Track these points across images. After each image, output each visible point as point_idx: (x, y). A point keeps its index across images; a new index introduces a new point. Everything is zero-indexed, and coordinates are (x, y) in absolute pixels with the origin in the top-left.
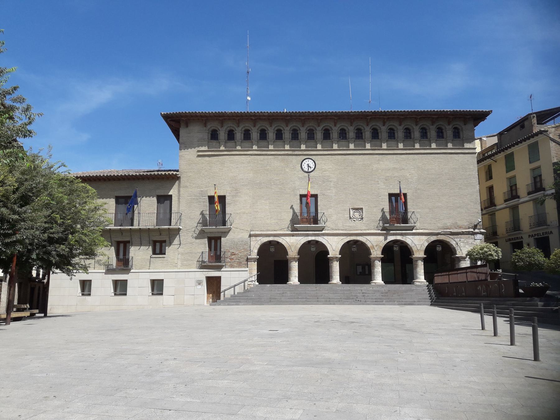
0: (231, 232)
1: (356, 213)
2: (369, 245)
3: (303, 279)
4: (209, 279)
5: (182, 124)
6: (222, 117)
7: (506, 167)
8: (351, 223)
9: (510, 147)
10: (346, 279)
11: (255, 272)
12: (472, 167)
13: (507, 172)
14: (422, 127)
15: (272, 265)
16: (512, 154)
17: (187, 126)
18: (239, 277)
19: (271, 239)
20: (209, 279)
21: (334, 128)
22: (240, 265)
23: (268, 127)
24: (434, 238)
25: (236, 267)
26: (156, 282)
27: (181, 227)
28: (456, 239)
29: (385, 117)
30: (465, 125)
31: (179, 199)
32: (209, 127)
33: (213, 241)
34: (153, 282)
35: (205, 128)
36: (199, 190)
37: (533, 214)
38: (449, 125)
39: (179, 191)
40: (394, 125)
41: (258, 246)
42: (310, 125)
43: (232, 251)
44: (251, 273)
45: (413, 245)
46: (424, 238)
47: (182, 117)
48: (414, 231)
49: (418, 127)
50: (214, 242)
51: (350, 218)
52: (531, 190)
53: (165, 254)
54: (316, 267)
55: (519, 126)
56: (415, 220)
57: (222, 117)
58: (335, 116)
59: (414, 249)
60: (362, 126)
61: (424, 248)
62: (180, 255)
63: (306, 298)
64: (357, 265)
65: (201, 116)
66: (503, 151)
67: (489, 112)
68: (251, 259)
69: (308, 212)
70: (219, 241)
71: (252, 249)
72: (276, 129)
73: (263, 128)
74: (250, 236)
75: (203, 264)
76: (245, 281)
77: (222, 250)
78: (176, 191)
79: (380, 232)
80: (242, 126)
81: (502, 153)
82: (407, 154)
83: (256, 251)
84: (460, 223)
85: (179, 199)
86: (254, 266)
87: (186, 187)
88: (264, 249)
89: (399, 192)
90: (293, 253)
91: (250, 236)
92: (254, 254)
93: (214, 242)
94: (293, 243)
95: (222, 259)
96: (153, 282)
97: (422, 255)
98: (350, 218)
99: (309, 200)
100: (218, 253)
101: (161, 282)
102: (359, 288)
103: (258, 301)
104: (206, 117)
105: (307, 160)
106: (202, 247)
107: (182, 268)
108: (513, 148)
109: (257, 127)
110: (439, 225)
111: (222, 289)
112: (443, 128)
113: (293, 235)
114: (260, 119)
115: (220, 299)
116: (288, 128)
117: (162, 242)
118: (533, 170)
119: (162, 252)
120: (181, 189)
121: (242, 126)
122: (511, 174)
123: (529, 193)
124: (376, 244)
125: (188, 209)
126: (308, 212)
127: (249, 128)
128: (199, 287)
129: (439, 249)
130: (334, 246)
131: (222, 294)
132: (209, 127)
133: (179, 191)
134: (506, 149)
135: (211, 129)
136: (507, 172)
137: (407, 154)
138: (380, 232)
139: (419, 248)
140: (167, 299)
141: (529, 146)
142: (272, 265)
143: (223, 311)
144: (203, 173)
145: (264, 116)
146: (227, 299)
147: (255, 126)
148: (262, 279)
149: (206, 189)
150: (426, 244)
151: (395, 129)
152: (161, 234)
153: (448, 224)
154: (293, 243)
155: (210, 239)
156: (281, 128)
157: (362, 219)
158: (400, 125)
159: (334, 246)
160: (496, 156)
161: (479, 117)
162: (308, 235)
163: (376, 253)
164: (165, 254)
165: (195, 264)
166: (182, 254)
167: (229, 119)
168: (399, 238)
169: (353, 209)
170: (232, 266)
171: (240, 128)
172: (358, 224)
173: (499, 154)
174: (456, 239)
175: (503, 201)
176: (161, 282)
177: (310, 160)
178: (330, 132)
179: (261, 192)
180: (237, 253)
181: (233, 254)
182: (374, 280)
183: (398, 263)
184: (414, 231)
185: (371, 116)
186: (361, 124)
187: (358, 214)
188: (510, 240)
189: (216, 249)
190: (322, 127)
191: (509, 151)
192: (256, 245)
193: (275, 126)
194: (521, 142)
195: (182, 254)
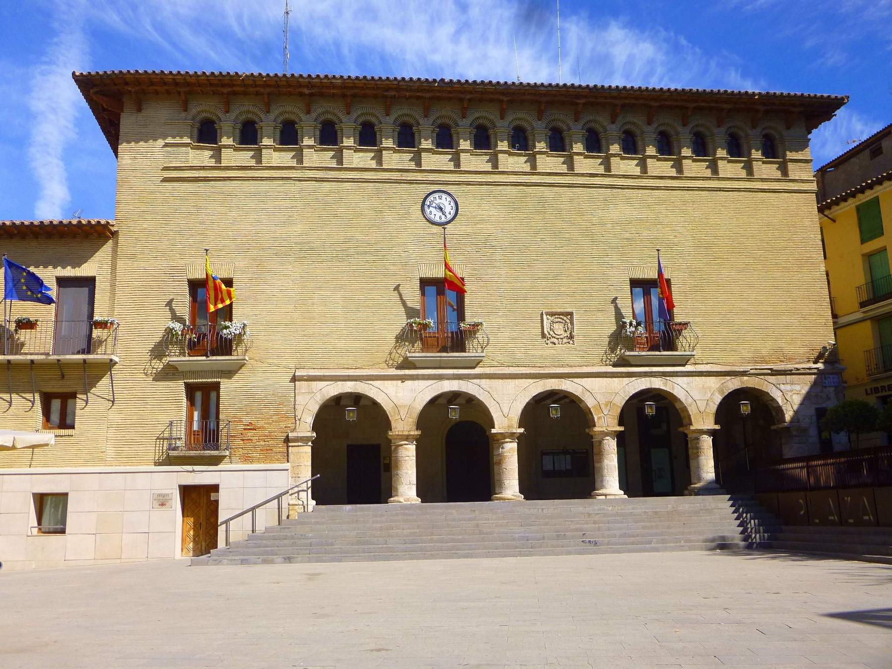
0: (243, 369)
1: (556, 326)
2: (590, 402)
3: (426, 492)
4: (187, 492)
5: (128, 104)
6: (228, 85)
7: (861, 232)
8: (549, 351)
9: (870, 187)
10: (533, 488)
11: (306, 473)
12: (807, 222)
13: (863, 241)
14: (696, 129)
15: (350, 458)
16: (876, 201)
17: (139, 110)
18: (265, 485)
19: (349, 387)
20: (187, 492)
21: (499, 123)
22: (267, 454)
23: (340, 115)
24: (734, 384)
25: (259, 461)
26: (48, 502)
27: (116, 359)
28: (782, 387)
29: (617, 102)
30: (788, 128)
31: (113, 286)
32: (194, 111)
33: (198, 395)
34: (41, 500)
35: (183, 114)
36: (165, 264)
37: (873, 347)
38: (754, 127)
39: (114, 268)
40: (634, 124)
41: (315, 408)
42: (444, 113)
43: (246, 420)
44: (296, 477)
45: (690, 400)
46: (712, 381)
47: (127, 84)
48: (688, 368)
49: (651, 129)
50: (203, 396)
51: (543, 336)
52: (865, 298)
53: (73, 427)
54: (460, 456)
55: (867, 152)
56: (693, 341)
57: (228, 85)
58: (503, 93)
59: (692, 410)
60: (564, 122)
61: (714, 408)
62: (111, 431)
63: (453, 540)
64: (544, 454)
65: (176, 83)
66: (854, 196)
67: (843, 99)
68: (297, 440)
69: (442, 317)
70: (213, 395)
71: (299, 414)
72: (361, 120)
73: (330, 117)
74: (294, 379)
75: (173, 453)
76: (278, 497)
77: (221, 417)
78: (107, 268)
79: (611, 369)
80: (277, 112)
81: (851, 201)
82: (667, 188)
83: (309, 420)
84: (789, 349)
85: (113, 286)
86: (304, 455)
87: (133, 257)
88: (331, 413)
89: (655, 276)
90: (403, 424)
91: (294, 379)
92: (305, 428)
93: (203, 396)
94: (404, 399)
95: (223, 439)
96: (41, 500)
97: (710, 424)
98: (543, 336)
99: (445, 289)
100: (212, 426)
101: (62, 498)
102: (581, 509)
103: (322, 550)
104: (188, 84)
105: (436, 195)
106: (171, 408)
107: (118, 469)
108: (878, 188)
109: (314, 115)
110: (746, 354)
111: (222, 518)
112: (742, 134)
113: (403, 378)
114: (322, 95)
115: (215, 546)
116: (391, 119)
117: (68, 397)
118: (868, 257)
119: (65, 423)
120: (120, 264)
121: (276, 111)
122: (874, 245)
123: (863, 305)
124: (605, 397)
125: (136, 301)
126: (442, 317)
127: (293, 117)
128: (159, 514)
129: (745, 408)
130: (505, 406)
131: (221, 530)
132: (194, 111)
133: (114, 268)
134: (862, 191)
135: (198, 118)
136: (863, 241)
137: (667, 188)
138: (611, 369)
139: (702, 409)
140: (78, 543)
141: (858, 209)
142: (350, 458)
143: (217, 573)
144: (178, 215)
145: (334, 86)
146: (238, 545)
147: (308, 112)
148: (323, 493)
149: (182, 262)
150: (718, 399)
151: (638, 132)
152: (63, 376)
153: (764, 352)
154: (404, 399)
155: (191, 390)
156: (373, 120)
157: (571, 337)
158: (649, 123)
159: (505, 406)
160: (835, 208)
161: (820, 110)
162: (440, 378)
163: (606, 422)
164: (73, 427)
165: (152, 450)
166: (118, 428)
167: (245, 94)
168: (657, 383)
169: (547, 314)
170: (247, 459)
171: (272, 116)
172: (561, 350)
173: (843, 204)
174: (782, 387)
175: (857, 306)
176: (62, 498)
177: (444, 196)
178: (491, 132)
179: (322, 273)
180: (261, 423)
181: (251, 427)
182: (602, 487)
183: (655, 446)
184: (688, 368)
185: (586, 97)
186: (562, 117)
187: (561, 326)
188: (876, 390)
189: (205, 416)
190: (471, 118)
191: (869, 195)
192: (309, 402)
193: (360, 112)
194: (845, 199)
195: (118, 428)
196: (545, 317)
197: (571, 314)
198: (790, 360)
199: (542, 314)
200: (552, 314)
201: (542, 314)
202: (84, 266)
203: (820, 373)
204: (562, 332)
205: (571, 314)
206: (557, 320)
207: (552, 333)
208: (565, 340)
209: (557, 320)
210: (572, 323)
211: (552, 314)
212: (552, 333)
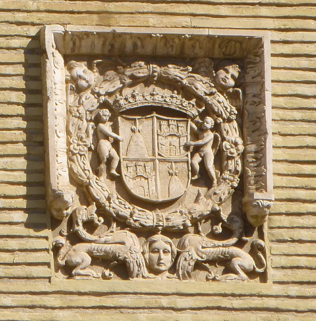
1: (137, 139)
51: (43, 208)
98: (43, 208)
157: (243, 222)
169: (74, 50)
187: (172, 138)
196: (56, 72)
197: (244, 54)
198: (201, 18)
199: (35, 52)
200: (113, 54)
201: (35, 52)
202: (41, 232)
203: (219, 113)
204: (180, 186)
205: (244, 54)
206: (143, 95)
207: (102, 187)
208: (200, 245)
209: (143, 95)
210: (251, 123)
211: (113, 54)
212: (102, 187)
